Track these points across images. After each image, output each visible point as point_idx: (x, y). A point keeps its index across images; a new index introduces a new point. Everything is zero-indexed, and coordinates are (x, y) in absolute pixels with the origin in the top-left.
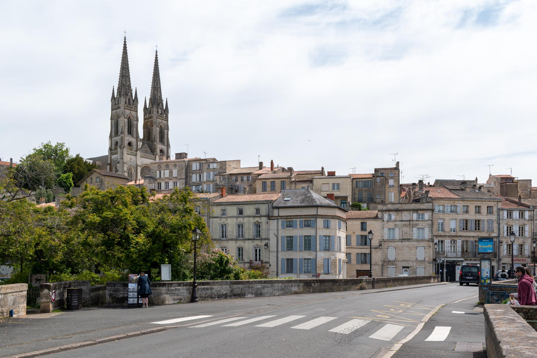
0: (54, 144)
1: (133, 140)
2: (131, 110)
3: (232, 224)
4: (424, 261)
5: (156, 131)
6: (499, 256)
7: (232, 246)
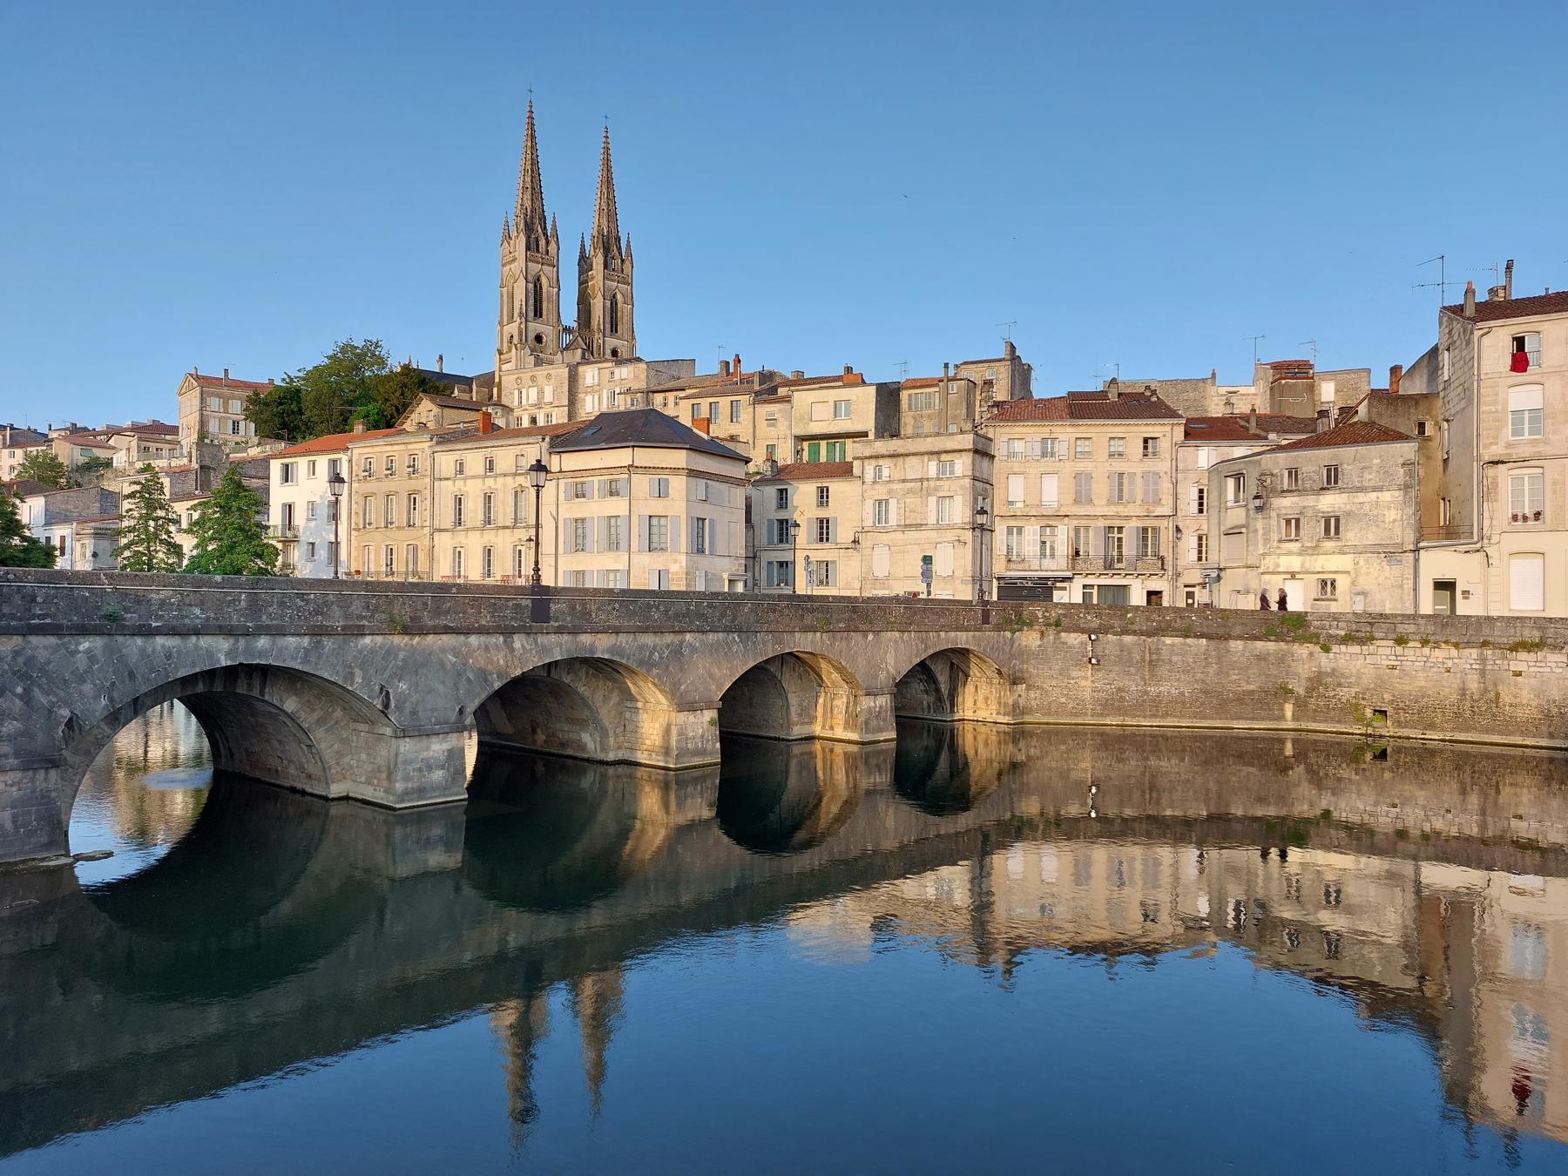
0: (359, 343)
3: (473, 492)
4: (952, 577)
6: (1175, 566)
7: (473, 544)
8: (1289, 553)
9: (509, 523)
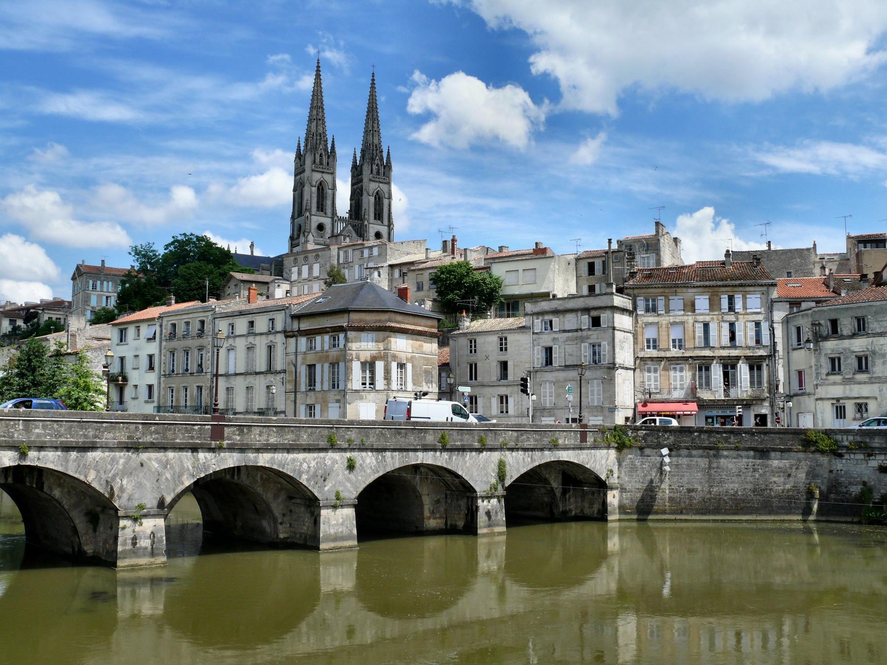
1: (327, 221)
2: (323, 172)
5: (368, 202)
8: (834, 384)
9: (263, 368)
